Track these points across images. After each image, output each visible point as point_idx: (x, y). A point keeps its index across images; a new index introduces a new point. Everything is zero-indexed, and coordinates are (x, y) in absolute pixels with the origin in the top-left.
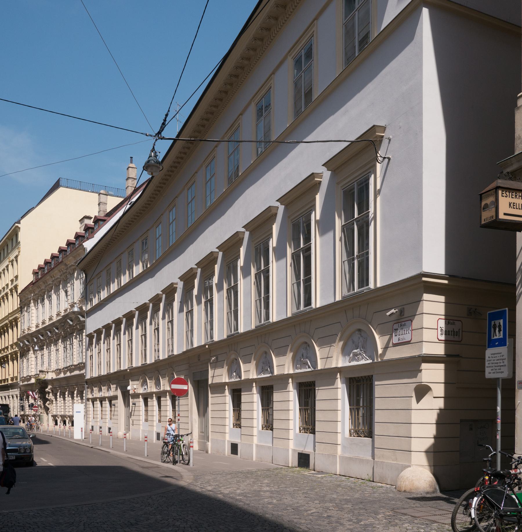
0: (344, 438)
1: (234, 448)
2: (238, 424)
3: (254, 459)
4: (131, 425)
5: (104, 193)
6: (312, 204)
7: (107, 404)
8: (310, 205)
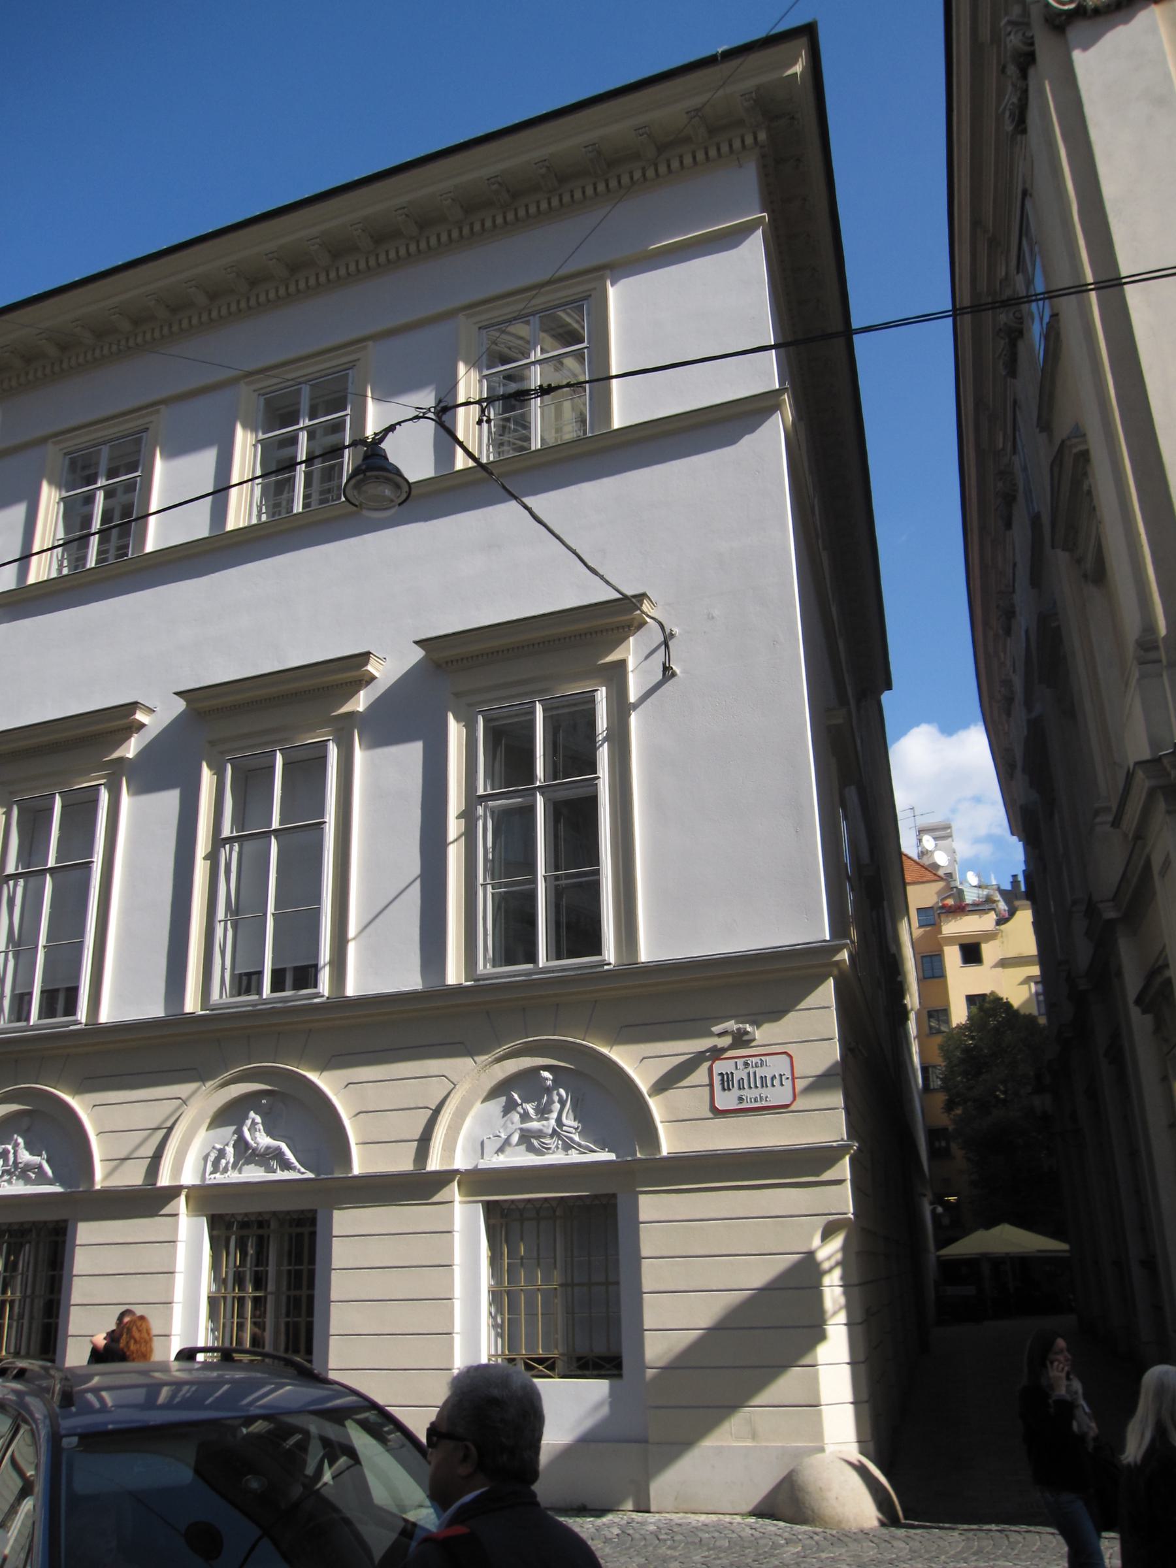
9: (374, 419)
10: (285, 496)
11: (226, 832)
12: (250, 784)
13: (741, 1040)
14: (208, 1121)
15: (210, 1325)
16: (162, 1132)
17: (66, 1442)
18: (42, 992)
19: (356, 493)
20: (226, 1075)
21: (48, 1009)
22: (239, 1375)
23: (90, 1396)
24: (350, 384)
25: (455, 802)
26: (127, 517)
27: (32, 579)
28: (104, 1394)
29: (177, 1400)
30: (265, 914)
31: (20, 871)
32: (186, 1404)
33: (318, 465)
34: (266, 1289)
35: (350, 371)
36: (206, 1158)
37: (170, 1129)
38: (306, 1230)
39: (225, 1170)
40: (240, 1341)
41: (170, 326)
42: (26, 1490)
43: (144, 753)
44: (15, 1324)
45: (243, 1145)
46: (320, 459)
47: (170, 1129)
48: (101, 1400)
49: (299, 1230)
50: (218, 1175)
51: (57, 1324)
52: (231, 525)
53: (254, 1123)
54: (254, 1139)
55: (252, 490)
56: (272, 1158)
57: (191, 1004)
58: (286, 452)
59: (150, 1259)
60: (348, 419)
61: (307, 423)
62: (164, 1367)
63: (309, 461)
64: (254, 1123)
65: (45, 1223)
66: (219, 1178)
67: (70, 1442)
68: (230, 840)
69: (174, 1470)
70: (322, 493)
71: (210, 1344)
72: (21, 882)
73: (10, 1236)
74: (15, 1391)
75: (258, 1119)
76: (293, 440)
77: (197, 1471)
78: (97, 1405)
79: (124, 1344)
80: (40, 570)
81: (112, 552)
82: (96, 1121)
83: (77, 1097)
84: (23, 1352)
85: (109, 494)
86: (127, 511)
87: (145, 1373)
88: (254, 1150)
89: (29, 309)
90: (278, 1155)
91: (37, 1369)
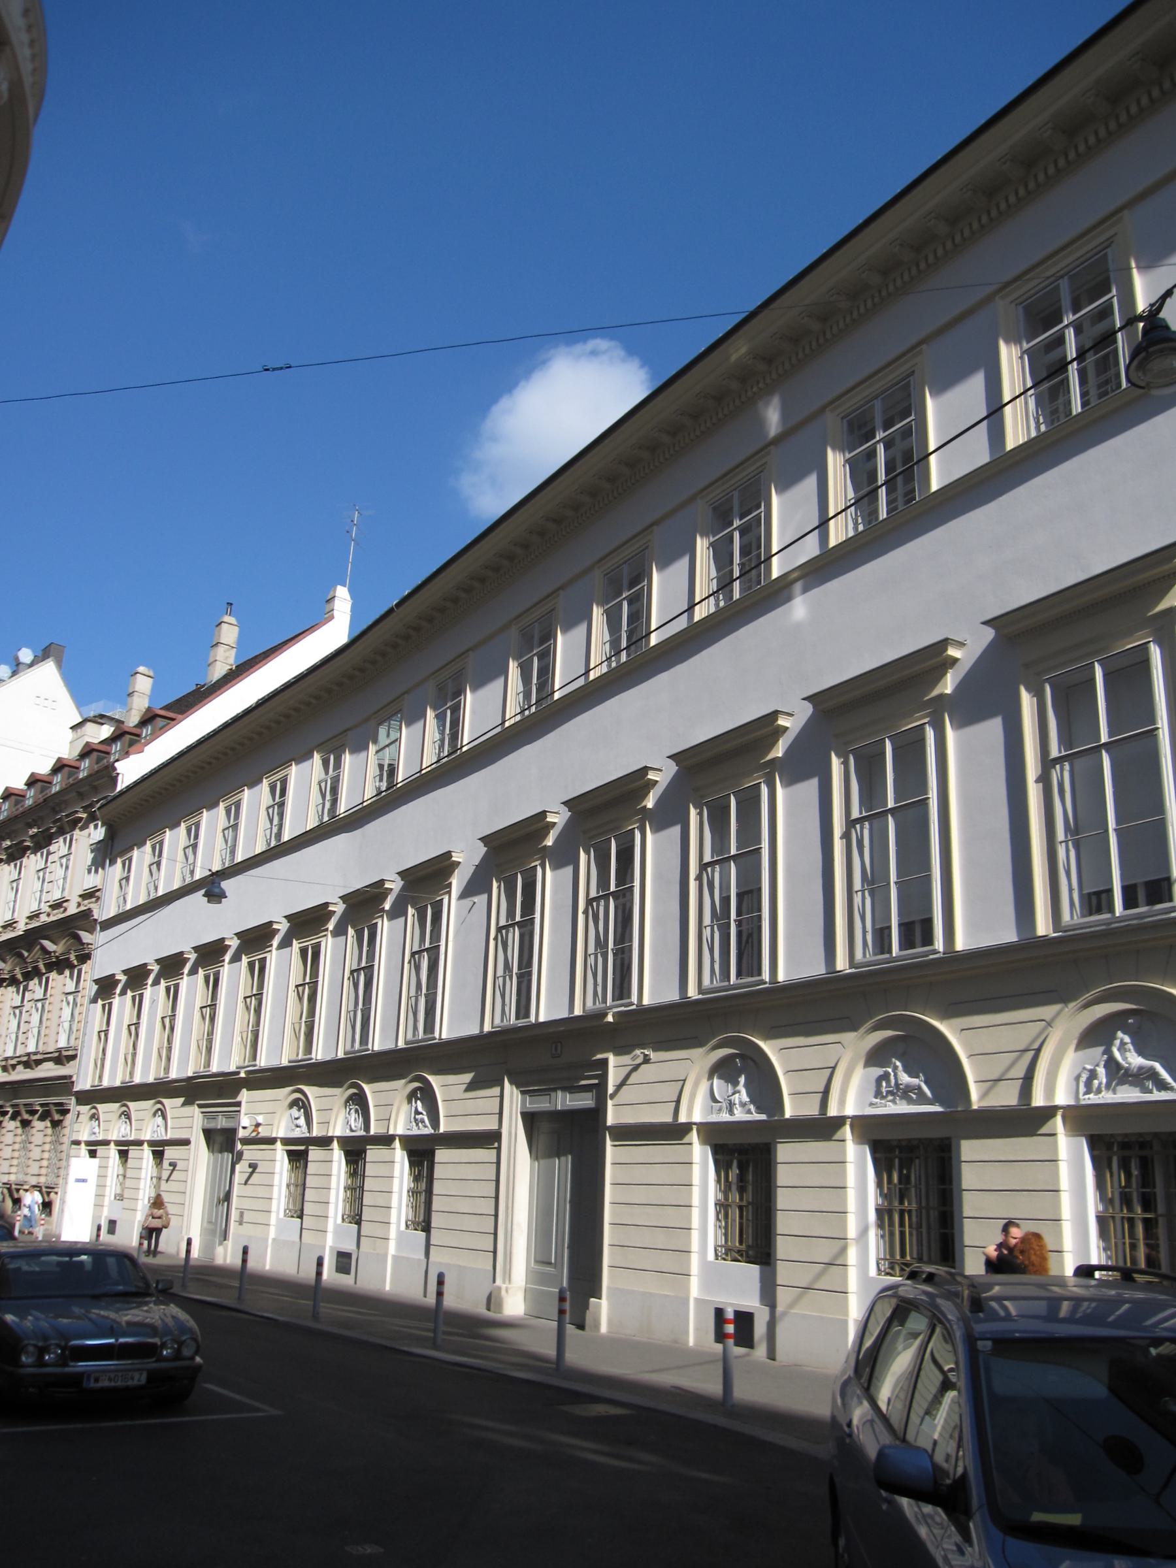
0: (278, 1219)
2: (356, 1218)
4: (233, 1225)
9: (1143, 291)
10: (1061, 400)
11: (1054, 752)
12: (1072, 702)
13: (647, 1060)
14: (1075, 1042)
15: (1101, 1244)
16: (1031, 1054)
17: (980, 1344)
18: (900, 925)
19: (1140, 374)
20: (1088, 996)
21: (907, 941)
22: (1140, 1295)
23: (994, 1304)
24: (1110, 262)
25: (1032, 770)
26: (909, 461)
27: (833, 542)
28: (1006, 1303)
29: (1078, 1315)
30: (1107, 831)
31: (864, 814)
32: (1087, 1320)
33: (1091, 358)
34: (1155, 1211)
35: (1109, 250)
36: (1077, 1078)
37: (1038, 1051)
39: (1099, 1091)
40: (1134, 1260)
41: (918, 265)
42: (946, 1385)
43: (960, 687)
44: (914, 1232)
45: (1113, 1065)
46: (1091, 352)
47: (1038, 1050)
48: (1005, 1308)
50: (1091, 1096)
51: (953, 1235)
52: (1010, 445)
53: (1123, 1044)
54: (1125, 1059)
55: (1026, 403)
56: (1148, 1078)
57: (1043, 927)
58: (1055, 355)
59: (1034, 1177)
60: (1115, 300)
61: (1071, 318)
62: (1061, 1281)
63: (1080, 357)
64: (1123, 1044)
65: (931, 1140)
66: (1093, 1099)
67: (985, 1345)
68: (858, 821)
69: (1087, 1384)
70: (1099, 386)
71: (1103, 1262)
72: (867, 825)
73: (900, 1152)
74: (925, 1293)
75: (1127, 1039)
76: (1060, 340)
77: (1111, 1389)
78: (1002, 1313)
79: (1017, 1259)
80: (838, 533)
81: (901, 500)
82: (965, 1045)
83: (945, 1022)
84: (925, 1258)
85: (888, 444)
86: (908, 456)
87: (1043, 1286)
88: (1127, 1070)
89: (788, 294)
90: (1153, 1075)
91: (943, 1274)
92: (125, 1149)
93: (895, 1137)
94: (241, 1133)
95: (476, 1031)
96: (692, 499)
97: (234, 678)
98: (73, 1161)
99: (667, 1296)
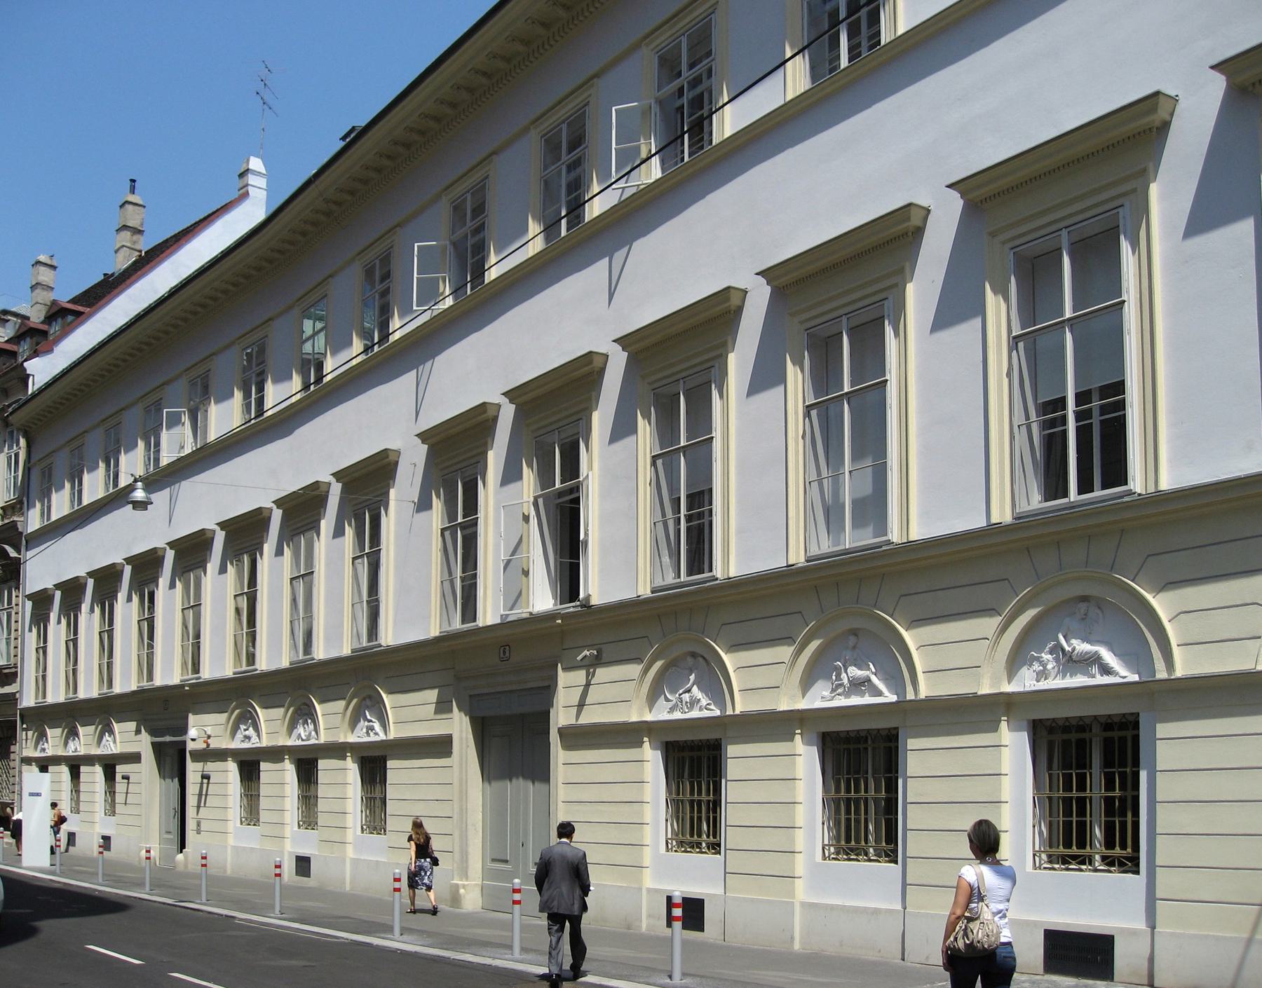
1: (303, 865)
3: (797, 946)
5: (49, 262)
6: (718, 352)
7: (94, 776)
8: (888, 283)
38: (1129, 734)
49: (1066, 736)
81: (865, 44)
90: (1096, 660)
92: (75, 766)
93: (1051, 716)
94: (190, 746)
95: (980, 523)
96: (636, 47)
97: (143, 266)
98: (25, 775)
99: (876, 911)
